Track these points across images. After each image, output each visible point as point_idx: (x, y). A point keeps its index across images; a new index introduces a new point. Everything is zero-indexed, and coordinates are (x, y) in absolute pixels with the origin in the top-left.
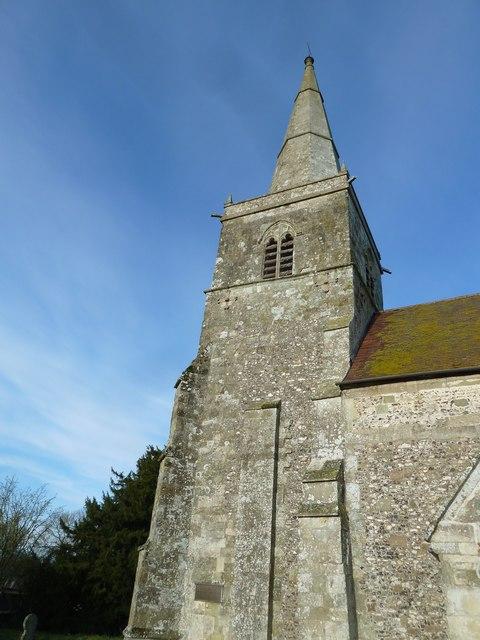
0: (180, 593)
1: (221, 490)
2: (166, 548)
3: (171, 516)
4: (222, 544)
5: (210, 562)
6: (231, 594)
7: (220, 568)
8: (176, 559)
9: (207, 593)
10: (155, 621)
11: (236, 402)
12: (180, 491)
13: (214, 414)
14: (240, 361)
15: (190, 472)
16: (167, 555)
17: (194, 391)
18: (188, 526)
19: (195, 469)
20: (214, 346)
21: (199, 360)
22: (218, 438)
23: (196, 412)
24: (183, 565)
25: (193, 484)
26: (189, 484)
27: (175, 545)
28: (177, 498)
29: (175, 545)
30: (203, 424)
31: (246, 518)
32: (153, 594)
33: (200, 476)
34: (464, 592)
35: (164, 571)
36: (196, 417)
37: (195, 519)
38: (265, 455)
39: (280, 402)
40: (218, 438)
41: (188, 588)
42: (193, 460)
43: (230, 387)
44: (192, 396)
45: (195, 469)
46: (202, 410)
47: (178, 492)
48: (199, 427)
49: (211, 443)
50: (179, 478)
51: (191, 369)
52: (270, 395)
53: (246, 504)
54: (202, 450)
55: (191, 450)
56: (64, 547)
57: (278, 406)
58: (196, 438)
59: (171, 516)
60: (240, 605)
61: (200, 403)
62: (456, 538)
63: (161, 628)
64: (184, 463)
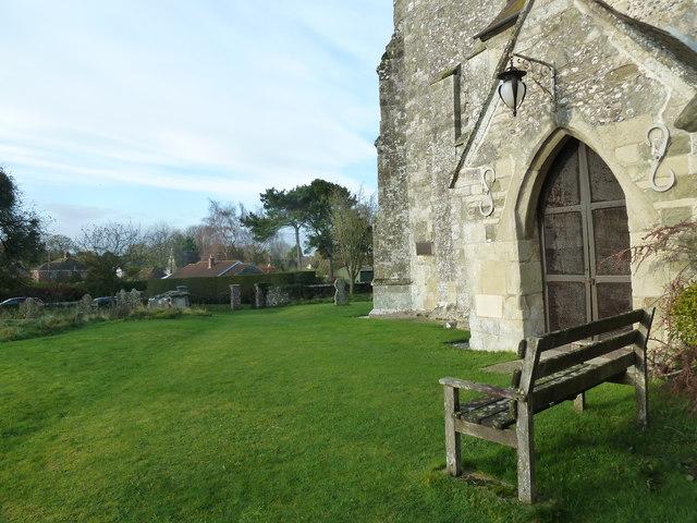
0: (407, 252)
1: (424, 165)
2: (390, 220)
3: (389, 195)
4: (429, 210)
5: (422, 225)
6: (435, 250)
7: (430, 230)
8: (400, 227)
9: (424, 249)
10: (390, 273)
11: (426, 77)
12: (394, 172)
13: (412, 95)
14: (426, 30)
15: (401, 154)
16: (392, 225)
17: (393, 78)
18: (406, 200)
19: (405, 150)
20: (405, 23)
21: (392, 44)
22: (417, 117)
23: (398, 98)
24: (407, 230)
25: (405, 164)
26: (401, 165)
27: (398, 217)
28: (393, 179)
29: (398, 217)
30: (407, 106)
31: (440, 185)
32: (386, 254)
33: (409, 157)
34: (473, 225)
35: (391, 237)
36: (398, 103)
37: (411, 193)
38: (448, 125)
39: (459, 66)
40: (417, 117)
41: (413, 250)
42: (402, 143)
43: (421, 63)
44: (391, 83)
45: (405, 150)
46: (403, 94)
47: (393, 174)
48: (403, 111)
49: (413, 124)
50: (392, 162)
51: (385, 56)
52: (452, 61)
53: (438, 173)
54: (409, 132)
55: (399, 134)
56: (39, 239)
57: (457, 72)
58: (402, 122)
59: (389, 195)
60: (441, 254)
61: (400, 87)
62: (470, 182)
63: (396, 277)
64: (393, 147)
